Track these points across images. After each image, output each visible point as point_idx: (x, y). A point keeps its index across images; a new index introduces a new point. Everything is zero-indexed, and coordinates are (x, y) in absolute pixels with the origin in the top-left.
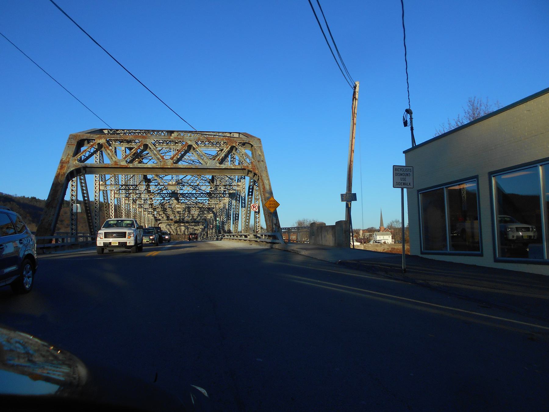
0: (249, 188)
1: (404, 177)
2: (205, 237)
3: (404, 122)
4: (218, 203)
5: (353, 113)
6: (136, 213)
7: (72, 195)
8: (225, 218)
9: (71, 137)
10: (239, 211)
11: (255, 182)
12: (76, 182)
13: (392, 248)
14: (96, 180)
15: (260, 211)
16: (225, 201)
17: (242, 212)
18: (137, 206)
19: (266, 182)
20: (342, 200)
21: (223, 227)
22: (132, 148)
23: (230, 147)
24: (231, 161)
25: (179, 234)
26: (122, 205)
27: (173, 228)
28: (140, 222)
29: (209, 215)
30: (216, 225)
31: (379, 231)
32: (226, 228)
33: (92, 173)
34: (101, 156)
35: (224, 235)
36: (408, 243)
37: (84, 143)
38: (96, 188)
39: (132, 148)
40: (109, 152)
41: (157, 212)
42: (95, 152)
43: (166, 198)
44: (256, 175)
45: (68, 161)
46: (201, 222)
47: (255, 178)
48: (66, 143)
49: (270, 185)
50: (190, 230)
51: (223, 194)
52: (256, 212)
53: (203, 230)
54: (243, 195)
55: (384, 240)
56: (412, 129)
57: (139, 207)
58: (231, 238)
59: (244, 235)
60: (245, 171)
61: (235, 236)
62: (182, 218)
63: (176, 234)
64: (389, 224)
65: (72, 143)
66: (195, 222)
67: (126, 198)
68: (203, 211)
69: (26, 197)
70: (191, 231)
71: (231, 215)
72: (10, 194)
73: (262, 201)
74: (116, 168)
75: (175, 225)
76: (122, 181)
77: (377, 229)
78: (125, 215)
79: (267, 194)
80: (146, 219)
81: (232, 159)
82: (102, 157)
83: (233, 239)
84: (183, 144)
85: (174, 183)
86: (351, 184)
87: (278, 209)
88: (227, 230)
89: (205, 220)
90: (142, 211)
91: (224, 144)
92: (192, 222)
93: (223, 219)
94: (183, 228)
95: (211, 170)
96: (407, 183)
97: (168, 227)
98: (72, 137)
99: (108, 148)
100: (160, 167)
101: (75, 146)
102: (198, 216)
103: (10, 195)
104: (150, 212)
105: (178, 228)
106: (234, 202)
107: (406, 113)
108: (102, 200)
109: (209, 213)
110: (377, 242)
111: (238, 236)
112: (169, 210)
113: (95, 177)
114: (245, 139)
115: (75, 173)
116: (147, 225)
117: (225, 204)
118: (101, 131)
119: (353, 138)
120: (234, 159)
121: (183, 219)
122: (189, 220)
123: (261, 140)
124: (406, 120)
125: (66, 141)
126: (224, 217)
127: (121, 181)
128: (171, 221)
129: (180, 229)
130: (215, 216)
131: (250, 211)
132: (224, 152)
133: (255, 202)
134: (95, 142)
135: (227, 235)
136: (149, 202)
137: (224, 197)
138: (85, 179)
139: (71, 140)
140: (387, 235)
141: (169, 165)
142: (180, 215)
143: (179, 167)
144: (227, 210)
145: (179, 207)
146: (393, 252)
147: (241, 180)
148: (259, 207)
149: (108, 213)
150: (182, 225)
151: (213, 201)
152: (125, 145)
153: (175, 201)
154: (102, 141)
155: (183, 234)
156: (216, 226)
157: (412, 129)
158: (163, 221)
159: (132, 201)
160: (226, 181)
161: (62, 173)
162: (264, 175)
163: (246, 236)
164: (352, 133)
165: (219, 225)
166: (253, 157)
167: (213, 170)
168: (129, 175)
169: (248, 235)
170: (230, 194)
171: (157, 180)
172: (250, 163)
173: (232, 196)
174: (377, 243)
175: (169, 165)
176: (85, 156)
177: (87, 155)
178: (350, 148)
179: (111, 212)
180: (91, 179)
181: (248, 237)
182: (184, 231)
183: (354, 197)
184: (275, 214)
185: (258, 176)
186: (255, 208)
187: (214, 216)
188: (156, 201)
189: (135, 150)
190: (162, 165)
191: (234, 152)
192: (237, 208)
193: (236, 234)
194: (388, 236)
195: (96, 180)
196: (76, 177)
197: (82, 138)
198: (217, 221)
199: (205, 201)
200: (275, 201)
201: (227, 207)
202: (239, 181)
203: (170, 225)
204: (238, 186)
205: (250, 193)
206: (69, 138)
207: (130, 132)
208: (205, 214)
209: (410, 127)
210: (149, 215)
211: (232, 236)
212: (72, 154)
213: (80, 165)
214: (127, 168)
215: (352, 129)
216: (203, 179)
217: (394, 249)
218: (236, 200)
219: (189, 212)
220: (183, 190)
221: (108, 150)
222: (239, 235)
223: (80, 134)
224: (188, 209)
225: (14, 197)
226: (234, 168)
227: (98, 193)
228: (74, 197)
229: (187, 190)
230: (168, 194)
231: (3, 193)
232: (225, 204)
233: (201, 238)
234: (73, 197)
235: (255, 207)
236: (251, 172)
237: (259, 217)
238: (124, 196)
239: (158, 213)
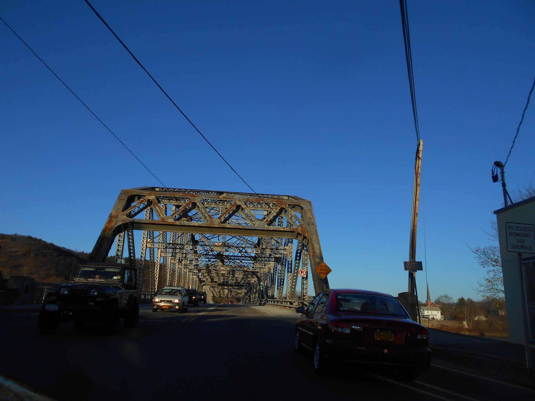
0: (297, 253)
1: (522, 238)
2: (247, 301)
3: (493, 177)
4: (263, 267)
5: (417, 174)
6: (174, 271)
7: (118, 250)
8: (269, 283)
9: (122, 192)
10: (284, 277)
11: (303, 246)
12: (123, 238)
13: (441, 325)
14: (144, 237)
15: (308, 278)
16: (270, 265)
17: (288, 277)
18: (183, 266)
19: (316, 246)
20: (406, 269)
21: (267, 292)
22: (180, 206)
23: (279, 208)
24: (278, 225)
25: (222, 297)
26: (168, 264)
27: (216, 291)
28: (184, 282)
29: (252, 279)
30: (260, 290)
31: (426, 305)
32: (270, 293)
33: (141, 229)
34: (151, 214)
35: (267, 300)
36: (459, 320)
37: (135, 199)
38: (143, 245)
39: (180, 206)
40: (158, 208)
41: (202, 273)
42: (146, 207)
43: (212, 260)
44: (306, 238)
45: (117, 216)
46: (245, 286)
47: (304, 242)
48: (117, 199)
49: (320, 250)
50: (233, 293)
51: (269, 258)
52: (303, 278)
53: (246, 294)
54: (290, 260)
55: (432, 315)
56: (504, 185)
57: (184, 268)
58: (275, 304)
59: (289, 302)
60: (294, 233)
61: (279, 302)
62: (226, 280)
63: (219, 297)
64: (437, 299)
65: (122, 198)
66: (238, 286)
67: (172, 257)
68: (247, 275)
69: (85, 252)
70: (234, 294)
71: (275, 280)
72: (71, 249)
73: (311, 266)
74: (164, 225)
75: (218, 288)
76: (170, 240)
77: (423, 303)
78: (170, 274)
79: (317, 259)
80: (190, 280)
81: (280, 223)
82: (152, 215)
83: (277, 305)
84: (232, 204)
85: (220, 244)
86: (414, 252)
87: (329, 276)
88: (270, 295)
89: (249, 283)
90: (188, 271)
91: (273, 205)
92: (236, 286)
93: (267, 284)
94: (226, 291)
95: (258, 231)
96: (526, 247)
97: (212, 289)
98: (123, 192)
99: (157, 204)
100: (206, 226)
101: (125, 201)
102: (242, 280)
103: (71, 250)
104: (195, 273)
105: (221, 291)
106: (279, 266)
107: (495, 166)
108: (148, 258)
109: (253, 277)
110: (424, 318)
111: (281, 302)
112: (214, 272)
113: (143, 234)
114: (296, 202)
115: (122, 228)
116: (190, 286)
117: (270, 269)
118: (153, 189)
119: (417, 200)
120: (282, 223)
121: (227, 282)
122: (233, 283)
123: (312, 203)
124: (497, 175)
125: (118, 196)
126: (269, 282)
127: (169, 240)
128: (215, 284)
129: (223, 292)
130: (259, 280)
131: (297, 276)
132: (275, 212)
133: (303, 267)
134: (145, 198)
135: (270, 301)
136: (194, 263)
137: (269, 261)
138: (133, 236)
139: (122, 196)
140: (436, 310)
141: (216, 225)
142: (224, 278)
143: (226, 227)
144: (271, 274)
145: (223, 270)
146: (444, 330)
147: (289, 244)
148: (307, 272)
149: (153, 271)
150: (226, 288)
151: (258, 265)
152: (174, 202)
153: (220, 264)
154: (152, 197)
155: (226, 297)
156: (259, 290)
157: (504, 185)
158: (207, 283)
159: (178, 260)
160: (272, 245)
161: (110, 227)
162: (314, 239)
163: (291, 303)
164: (415, 195)
165: (263, 290)
166: (303, 220)
167: (261, 231)
168: (178, 233)
169: (294, 302)
170: (276, 258)
171: (204, 241)
172: (299, 226)
173: (278, 260)
174: (425, 319)
175: (216, 225)
176: (134, 211)
177: (136, 211)
178: (413, 211)
179: (156, 270)
180: (139, 235)
181: (294, 304)
182: (227, 294)
183: (419, 266)
184: (326, 281)
185: (308, 240)
186: (303, 273)
187: (257, 280)
188: (201, 262)
189: (183, 208)
190: (209, 224)
191: (283, 213)
192: (282, 273)
193: (280, 300)
194: (436, 312)
195: (144, 237)
196: (123, 232)
197: (133, 194)
198: (261, 285)
199: (249, 265)
200: (326, 266)
201: (272, 271)
202: (286, 245)
203: (213, 287)
204: (285, 250)
205: (298, 258)
206: (121, 194)
207: (180, 191)
208: (249, 278)
209: (501, 182)
210: (194, 276)
211: (276, 302)
212: (121, 209)
213: (128, 220)
214: (173, 225)
215: (415, 190)
216: (249, 243)
217: (444, 325)
218: (282, 265)
219: (233, 275)
220: (229, 251)
221: (156, 207)
222: (284, 301)
223: (131, 190)
224: (233, 272)
225: (74, 252)
226: (282, 230)
227: (145, 250)
228: (120, 252)
229: (232, 252)
230: (213, 255)
231: (66, 248)
232: (270, 269)
233: (243, 302)
234: (119, 253)
235: (303, 272)
236: (301, 235)
237: (306, 284)
238: (170, 255)
239: (203, 274)
